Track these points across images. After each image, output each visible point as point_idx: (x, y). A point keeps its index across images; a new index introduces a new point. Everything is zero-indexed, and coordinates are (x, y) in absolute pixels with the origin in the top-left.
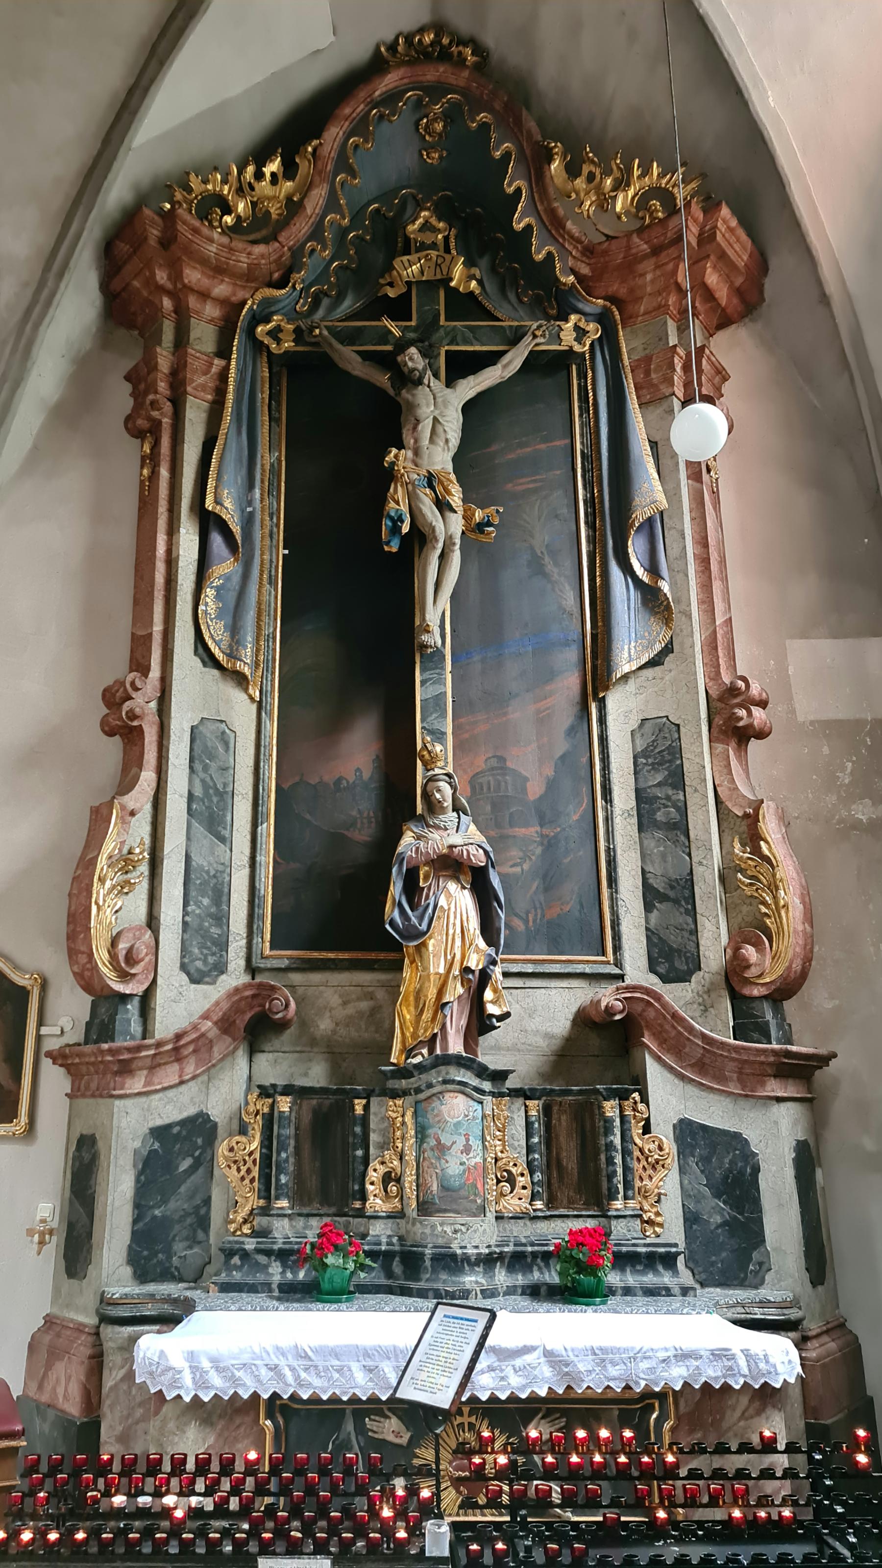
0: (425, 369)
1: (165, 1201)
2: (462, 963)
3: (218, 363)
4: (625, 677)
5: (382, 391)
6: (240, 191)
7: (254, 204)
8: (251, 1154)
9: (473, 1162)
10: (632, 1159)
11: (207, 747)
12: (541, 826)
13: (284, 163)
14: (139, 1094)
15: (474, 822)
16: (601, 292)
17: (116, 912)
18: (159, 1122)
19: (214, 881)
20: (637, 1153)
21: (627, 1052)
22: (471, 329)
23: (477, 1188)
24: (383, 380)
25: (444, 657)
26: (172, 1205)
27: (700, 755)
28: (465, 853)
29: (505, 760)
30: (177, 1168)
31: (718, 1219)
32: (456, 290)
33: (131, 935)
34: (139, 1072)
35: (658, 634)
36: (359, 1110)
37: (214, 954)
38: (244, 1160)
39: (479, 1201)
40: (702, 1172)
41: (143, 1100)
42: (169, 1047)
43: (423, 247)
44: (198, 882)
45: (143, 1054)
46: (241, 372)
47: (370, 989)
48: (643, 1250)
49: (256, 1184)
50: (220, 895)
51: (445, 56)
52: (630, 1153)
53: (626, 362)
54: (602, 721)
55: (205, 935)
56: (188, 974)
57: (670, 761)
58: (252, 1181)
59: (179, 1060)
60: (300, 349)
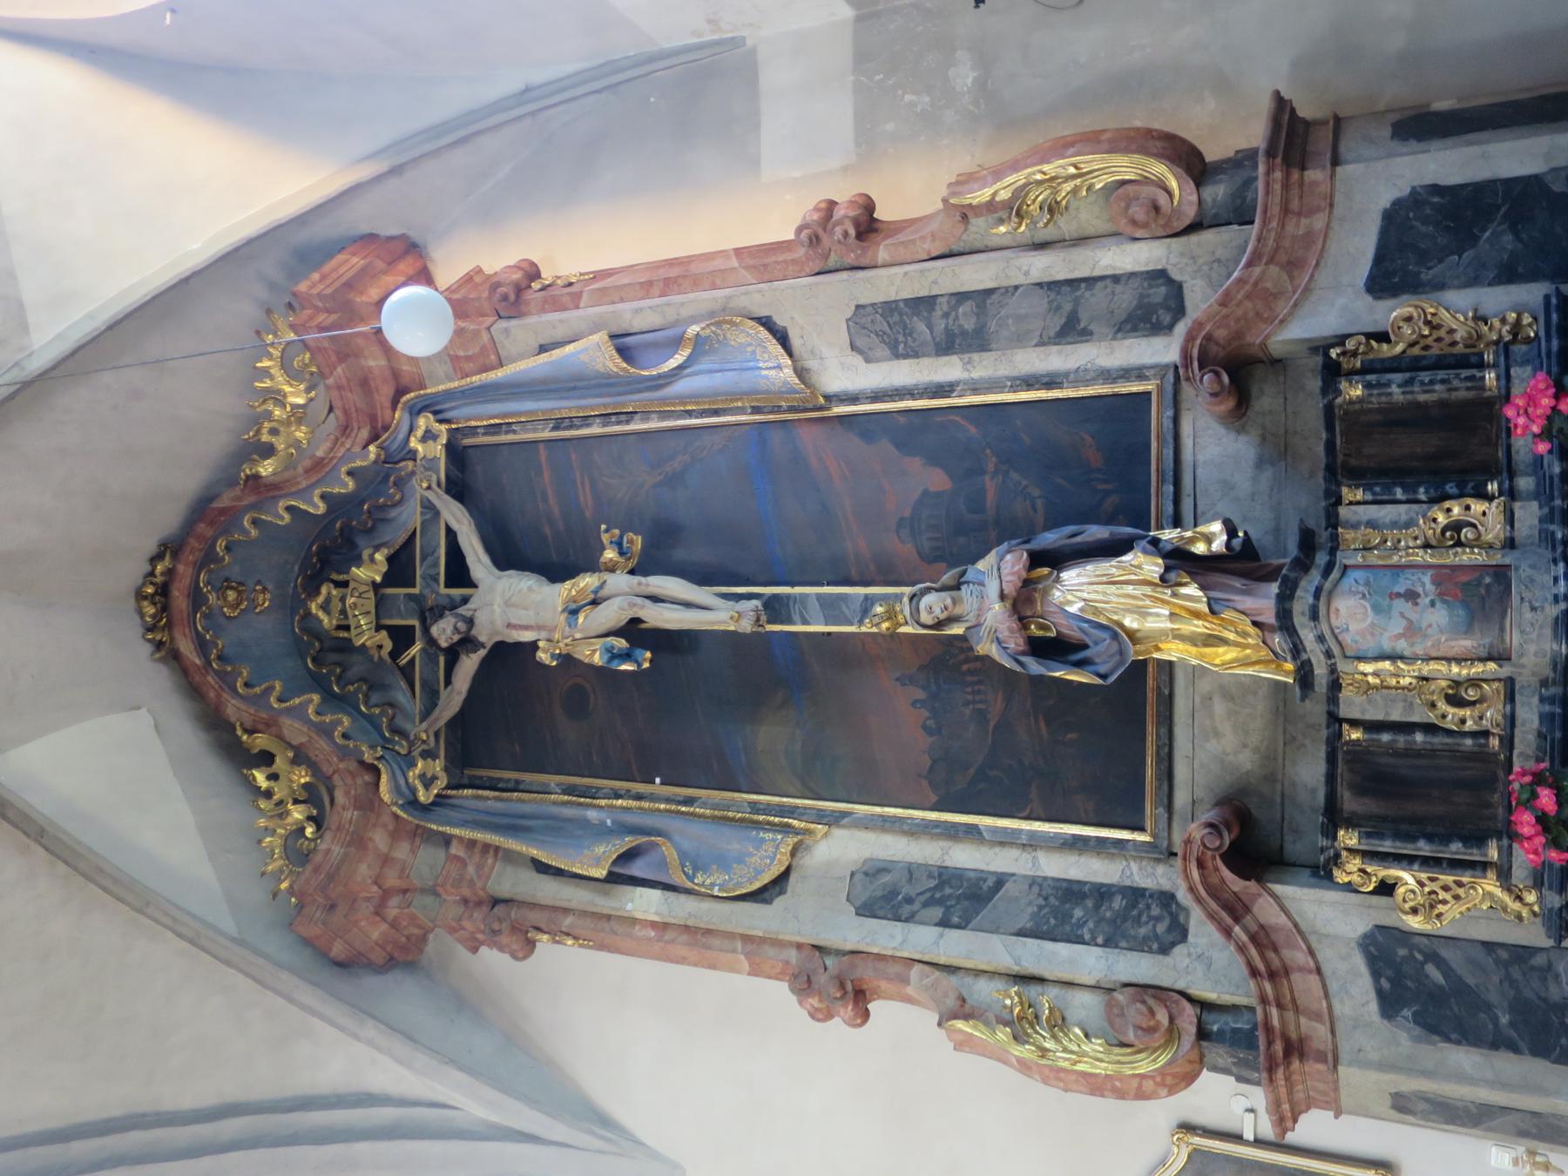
0: (457, 615)
1: (1488, 1007)
2: (1156, 585)
3: (456, 849)
4: (801, 373)
5: (485, 662)
6: (284, 815)
7: (296, 802)
8: (1421, 884)
9: (1430, 587)
10: (1424, 357)
11: (883, 897)
12: (984, 472)
13: (257, 766)
14: (1333, 1032)
15: (974, 562)
16: (388, 412)
17: (1087, 1036)
18: (1374, 1006)
19: (1052, 900)
20: (1416, 351)
21: (1280, 361)
22: (423, 559)
23: (1467, 584)
24: (469, 665)
25: (775, 596)
26: (1493, 997)
27: (892, 283)
28: (1010, 578)
29: (902, 519)
30: (1441, 988)
31: (1508, 239)
32: (386, 576)
33: (1117, 1020)
34: (1303, 1029)
35: (748, 335)
36: (1356, 735)
37: (1148, 907)
38: (1430, 893)
39: (1488, 580)
40: (1441, 261)
41: (1340, 1028)
42: (1268, 987)
43: (343, 612)
44: (1053, 921)
45: (1276, 1022)
46: (463, 824)
47: (1197, 699)
48: (1555, 344)
49: (1465, 880)
50: (1071, 892)
51: (164, 590)
52: (1417, 359)
53: (456, 384)
54: (854, 399)
55: (1123, 916)
56: (1174, 944)
57: (901, 315)
58: (1460, 884)
59: (1287, 972)
60: (442, 753)
